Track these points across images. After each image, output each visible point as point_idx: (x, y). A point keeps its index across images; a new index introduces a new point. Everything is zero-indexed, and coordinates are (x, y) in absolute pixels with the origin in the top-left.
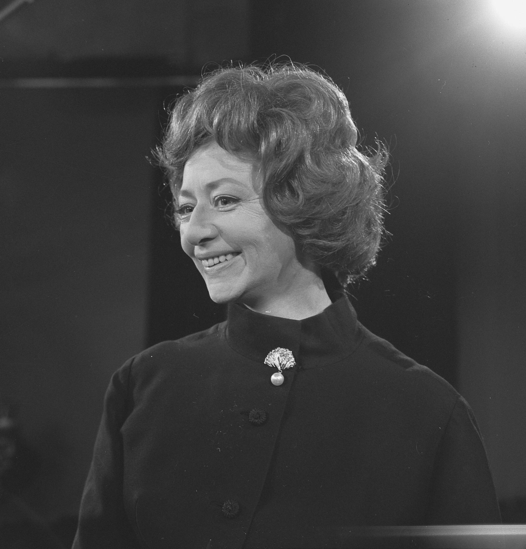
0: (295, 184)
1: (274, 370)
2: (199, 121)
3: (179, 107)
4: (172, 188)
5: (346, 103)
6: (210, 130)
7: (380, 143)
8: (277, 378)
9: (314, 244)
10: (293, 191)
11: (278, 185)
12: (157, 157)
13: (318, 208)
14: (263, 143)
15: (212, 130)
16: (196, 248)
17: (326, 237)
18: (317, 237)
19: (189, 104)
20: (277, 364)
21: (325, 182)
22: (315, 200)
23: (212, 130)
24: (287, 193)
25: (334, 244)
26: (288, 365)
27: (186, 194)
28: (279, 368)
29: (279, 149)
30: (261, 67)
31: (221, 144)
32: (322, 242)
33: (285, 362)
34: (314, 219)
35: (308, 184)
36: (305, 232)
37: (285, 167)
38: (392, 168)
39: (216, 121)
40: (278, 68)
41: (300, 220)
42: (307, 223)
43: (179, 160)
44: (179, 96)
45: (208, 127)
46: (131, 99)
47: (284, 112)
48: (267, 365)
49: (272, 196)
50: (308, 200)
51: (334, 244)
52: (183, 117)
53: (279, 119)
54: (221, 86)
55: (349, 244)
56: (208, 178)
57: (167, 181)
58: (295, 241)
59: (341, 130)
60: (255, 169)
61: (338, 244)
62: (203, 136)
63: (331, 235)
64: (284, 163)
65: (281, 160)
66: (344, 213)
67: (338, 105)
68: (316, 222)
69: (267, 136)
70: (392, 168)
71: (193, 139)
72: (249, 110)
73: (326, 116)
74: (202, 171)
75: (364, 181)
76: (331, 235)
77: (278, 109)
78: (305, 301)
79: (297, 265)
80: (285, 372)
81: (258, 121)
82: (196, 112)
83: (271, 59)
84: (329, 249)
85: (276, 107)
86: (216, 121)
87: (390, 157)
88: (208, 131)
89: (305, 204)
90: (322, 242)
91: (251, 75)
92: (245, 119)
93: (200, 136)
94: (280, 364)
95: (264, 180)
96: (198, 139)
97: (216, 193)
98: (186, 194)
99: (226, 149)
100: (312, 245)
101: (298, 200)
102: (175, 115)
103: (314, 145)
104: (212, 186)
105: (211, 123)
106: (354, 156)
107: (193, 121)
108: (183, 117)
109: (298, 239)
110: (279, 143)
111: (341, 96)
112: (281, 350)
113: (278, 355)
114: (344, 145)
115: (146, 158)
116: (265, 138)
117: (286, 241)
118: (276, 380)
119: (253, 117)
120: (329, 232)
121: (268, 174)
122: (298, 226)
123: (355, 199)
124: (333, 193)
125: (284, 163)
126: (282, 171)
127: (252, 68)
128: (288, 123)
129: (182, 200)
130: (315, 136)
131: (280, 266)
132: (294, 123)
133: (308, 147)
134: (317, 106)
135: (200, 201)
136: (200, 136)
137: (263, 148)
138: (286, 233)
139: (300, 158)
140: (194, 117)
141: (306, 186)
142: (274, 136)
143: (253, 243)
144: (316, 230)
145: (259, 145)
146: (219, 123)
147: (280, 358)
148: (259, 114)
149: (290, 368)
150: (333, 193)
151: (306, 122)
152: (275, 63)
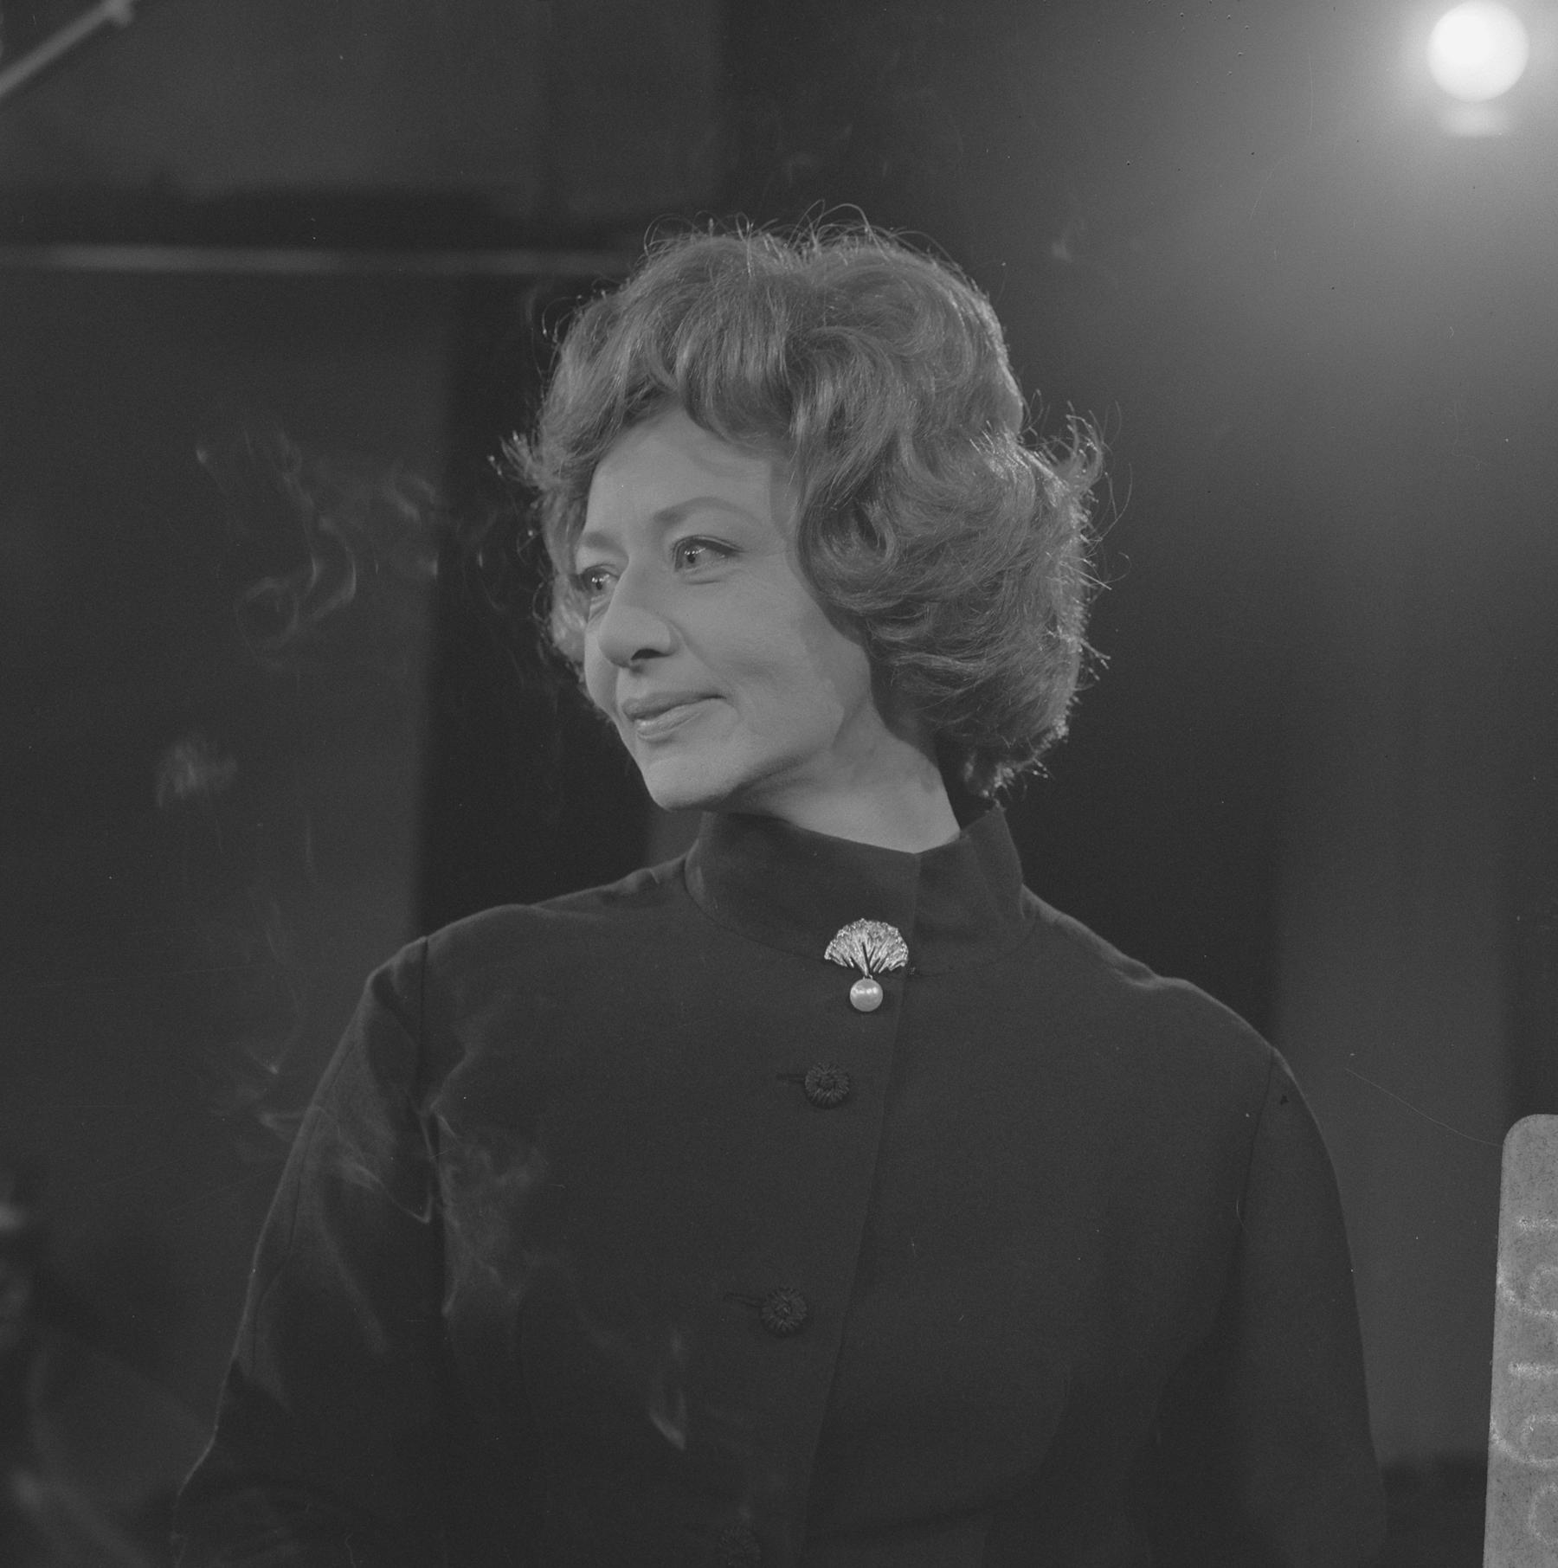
0: (875, 511)
1: (854, 974)
2: (637, 361)
3: (579, 331)
4: (550, 541)
5: (995, 327)
6: (667, 379)
7: (1079, 423)
8: (865, 993)
9: (921, 668)
10: (870, 534)
11: (839, 511)
12: (515, 461)
13: (929, 575)
14: (801, 411)
15: (676, 381)
16: (623, 675)
17: (955, 647)
18: (929, 646)
19: (610, 319)
20: (860, 957)
21: (948, 509)
22: (924, 553)
23: (676, 381)
24: (855, 536)
25: (970, 667)
26: (892, 963)
27: (599, 541)
28: (865, 969)
29: (837, 432)
30: (786, 237)
31: (694, 410)
32: (938, 662)
33: (881, 954)
34: (922, 601)
35: (908, 513)
36: (901, 635)
37: (853, 472)
38: (1110, 483)
39: (683, 358)
40: (828, 239)
41: (891, 604)
42: (904, 613)
43: (582, 458)
44: (582, 302)
45: (660, 372)
46: (463, 318)
47: (852, 335)
48: (832, 963)
49: (822, 542)
50: (908, 552)
51: (970, 667)
52: (593, 353)
53: (839, 351)
54: (697, 274)
55: (1005, 669)
56: (659, 499)
57: (538, 526)
58: (871, 660)
59: (984, 397)
60: (777, 475)
61: (977, 668)
62: (647, 396)
63: (962, 644)
64: (850, 459)
65: (843, 454)
66: (995, 587)
67: (977, 330)
68: (927, 607)
69: (811, 393)
70: (1110, 483)
71: (621, 400)
72: (768, 330)
73: (950, 354)
74: (637, 490)
75: (1047, 510)
76: (962, 644)
77: (835, 330)
78: (894, 810)
79: (871, 720)
80: (883, 977)
81: (788, 356)
82: (625, 351)
83: (814, 214)
84: (953, 679)
85: (830, 323)
86: (683, 358)
87: (1107, 457)
88: (661, 384)
89: (899, 563)
90: (938, 662)
91: (763, 253)
92: (757, 358)
93: (639, 395)
94: (868, 961)
95: (801, 502)
96: (638, 405)
97: (680, 533)
98: (599, 541)
99: (708, 427)
100: (917, 668)
101: (882, 555)
102: (568, 353)
103: (922, 421)
104: (669, 518)
105: (670, 366)
106: (1010, 458)
107: (623, 359)
108: (593, 353)
109: (879, 655)
110: (839, 414)
111: (986, 311)
112: (870, 925)
113: (865, 938)
114: (993, 427)
115: (488, 463)
116: (806, 394)
117: (851, 656)
118: (867, 998)
119: (776, 349)
120: (957, 636)
121: (809, 491)
122: (882, 618)
123: (1022, 553)
124: (970, 535)
125: (850, 459)
126: (846, 480)
127: (768, 240)
128: (862, 365)
129: (586, 558)
130: (924, 401)
131: (839, 717)
132: (874, 363)
133: (909, 424)
134: (926, 336)
135: (635, 556)
136: (639, 395)
137: (801, 423)
138: (853, 639)
139: (889, 450)
140: (628, 350)
141: (904, 519)
142: (826, 395)
143: (756, 669)
144: (925, 628)
145: (788, 413)
146: (693, 361)
147: (869, 946)
148: (792, 341)
149: (898, 970)
150: (970, 535)
151: (905, 365)
152: (825, 221)
